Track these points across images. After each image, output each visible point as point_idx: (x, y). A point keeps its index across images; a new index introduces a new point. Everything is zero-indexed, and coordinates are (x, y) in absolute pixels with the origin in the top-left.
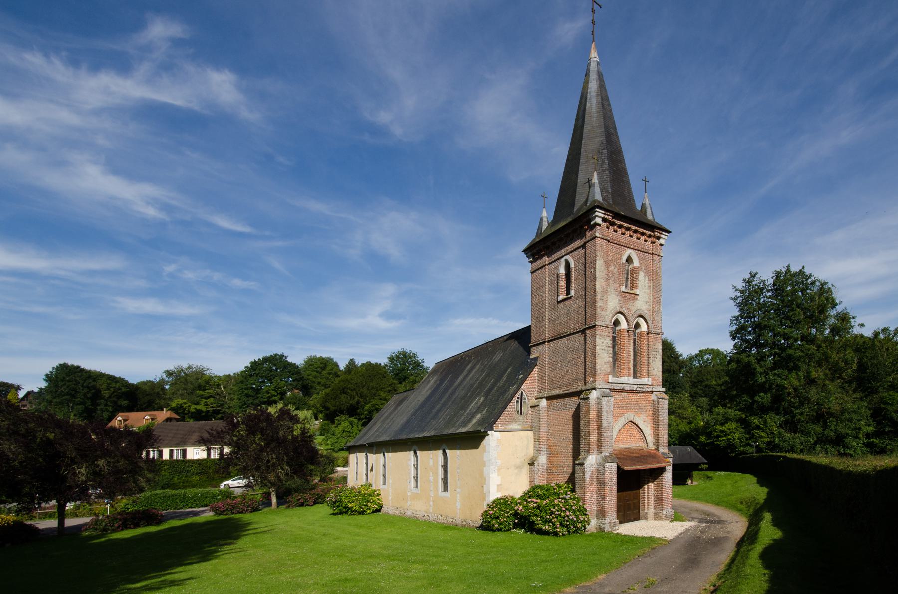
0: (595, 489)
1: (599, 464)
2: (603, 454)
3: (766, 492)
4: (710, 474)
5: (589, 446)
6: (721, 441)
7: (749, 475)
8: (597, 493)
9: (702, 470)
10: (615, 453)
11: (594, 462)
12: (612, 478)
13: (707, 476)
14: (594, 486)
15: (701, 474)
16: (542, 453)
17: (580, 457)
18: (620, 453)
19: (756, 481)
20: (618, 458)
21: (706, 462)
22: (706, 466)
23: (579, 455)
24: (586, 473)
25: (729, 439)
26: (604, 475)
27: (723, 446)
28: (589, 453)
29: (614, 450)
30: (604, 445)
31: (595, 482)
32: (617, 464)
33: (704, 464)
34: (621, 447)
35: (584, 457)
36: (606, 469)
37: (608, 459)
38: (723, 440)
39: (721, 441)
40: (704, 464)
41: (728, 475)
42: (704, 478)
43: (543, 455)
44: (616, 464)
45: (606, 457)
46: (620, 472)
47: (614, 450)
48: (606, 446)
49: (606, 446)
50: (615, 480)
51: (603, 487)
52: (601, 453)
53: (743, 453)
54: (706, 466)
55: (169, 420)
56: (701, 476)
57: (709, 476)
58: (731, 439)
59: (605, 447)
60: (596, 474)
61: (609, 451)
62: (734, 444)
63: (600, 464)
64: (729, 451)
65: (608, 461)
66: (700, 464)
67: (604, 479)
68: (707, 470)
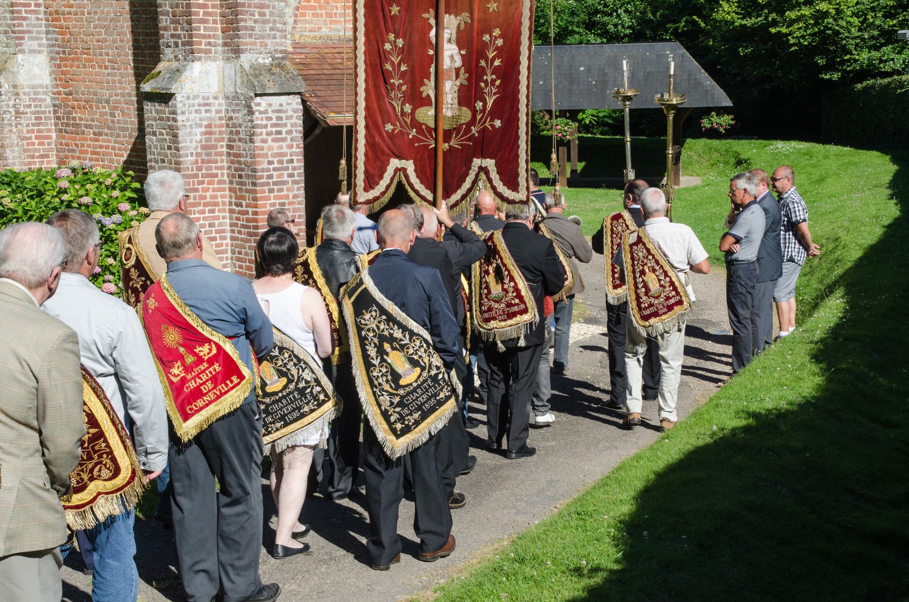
0: (224, 197)
1: (232, 99)
2: (246, 59)
3: (887, 221)
4: (747, 148)
5: (189, 23)
6: (791, 23)
7: (875, 153)
8: (232, 211)
9: (713, 134)
10: (298, 58)
11: (214, 88)
12: (283, 155)
13: (737, 155)
14: (221, 182)
15: (717, 151)
16: (28, 44)
17: (161, 66)
18: (321, 59)
19: (888, 178)
20: (306, 78)
21: (728, 103)
22: (726, 120)
23: (157, 60)
24: (181, 133)
25: (821, 16)
26: (252, 141)
27: (799, 44)
28: (190, 52)
29: (296, 45)
30: (247, 21)
31: (222, 168)
32: (304, 102)
33: (721, 111)
34: (325, 31)
35: (174, 65)
36: (258, 119)
37: (265, 78)
38: (798, 19)
39: (791, 23)
40: (721, 111)
41: (807, 153)
42: (726, 163)
43: (32, 52)
44: (298, 99)
45: (257, 70)
46: (317, 131)
47: (296, 45)
48: (258, 27)
49: (258, 27)
50: (299, 163)
51: (250, 187)
52: (237, 52)
53: (869, 71)
54: (726, 120)
55: (340, 214)
56: (715, 156)
57: (742, 157)
58: (826, 14)
59: (253, 29)
60: (226, 137)
61: (270, 47)
62: (837, 33)
63: (236, 97)
64: (821, 61)
65: (263, 86)
66: (706, 111)
67: (253, 156)
68: (732, 133)
